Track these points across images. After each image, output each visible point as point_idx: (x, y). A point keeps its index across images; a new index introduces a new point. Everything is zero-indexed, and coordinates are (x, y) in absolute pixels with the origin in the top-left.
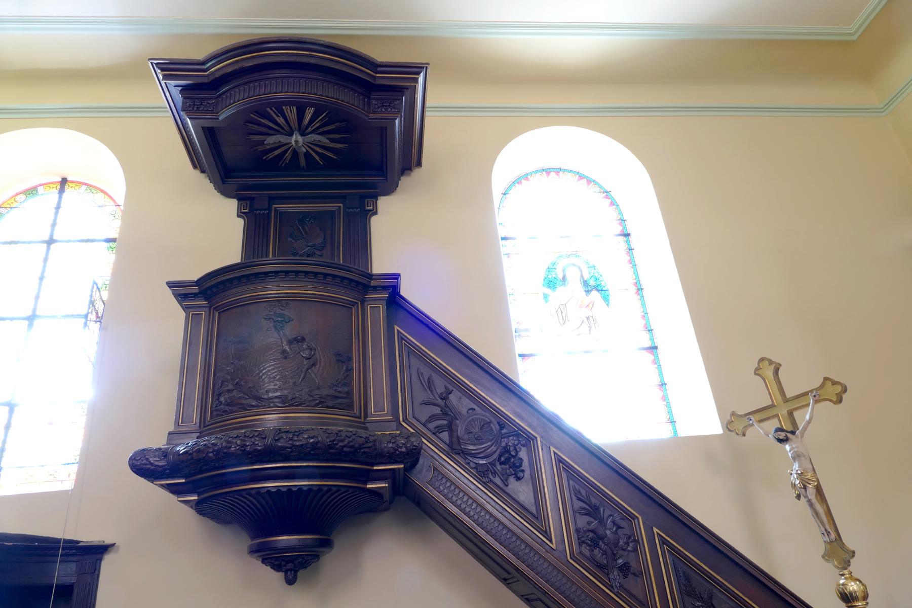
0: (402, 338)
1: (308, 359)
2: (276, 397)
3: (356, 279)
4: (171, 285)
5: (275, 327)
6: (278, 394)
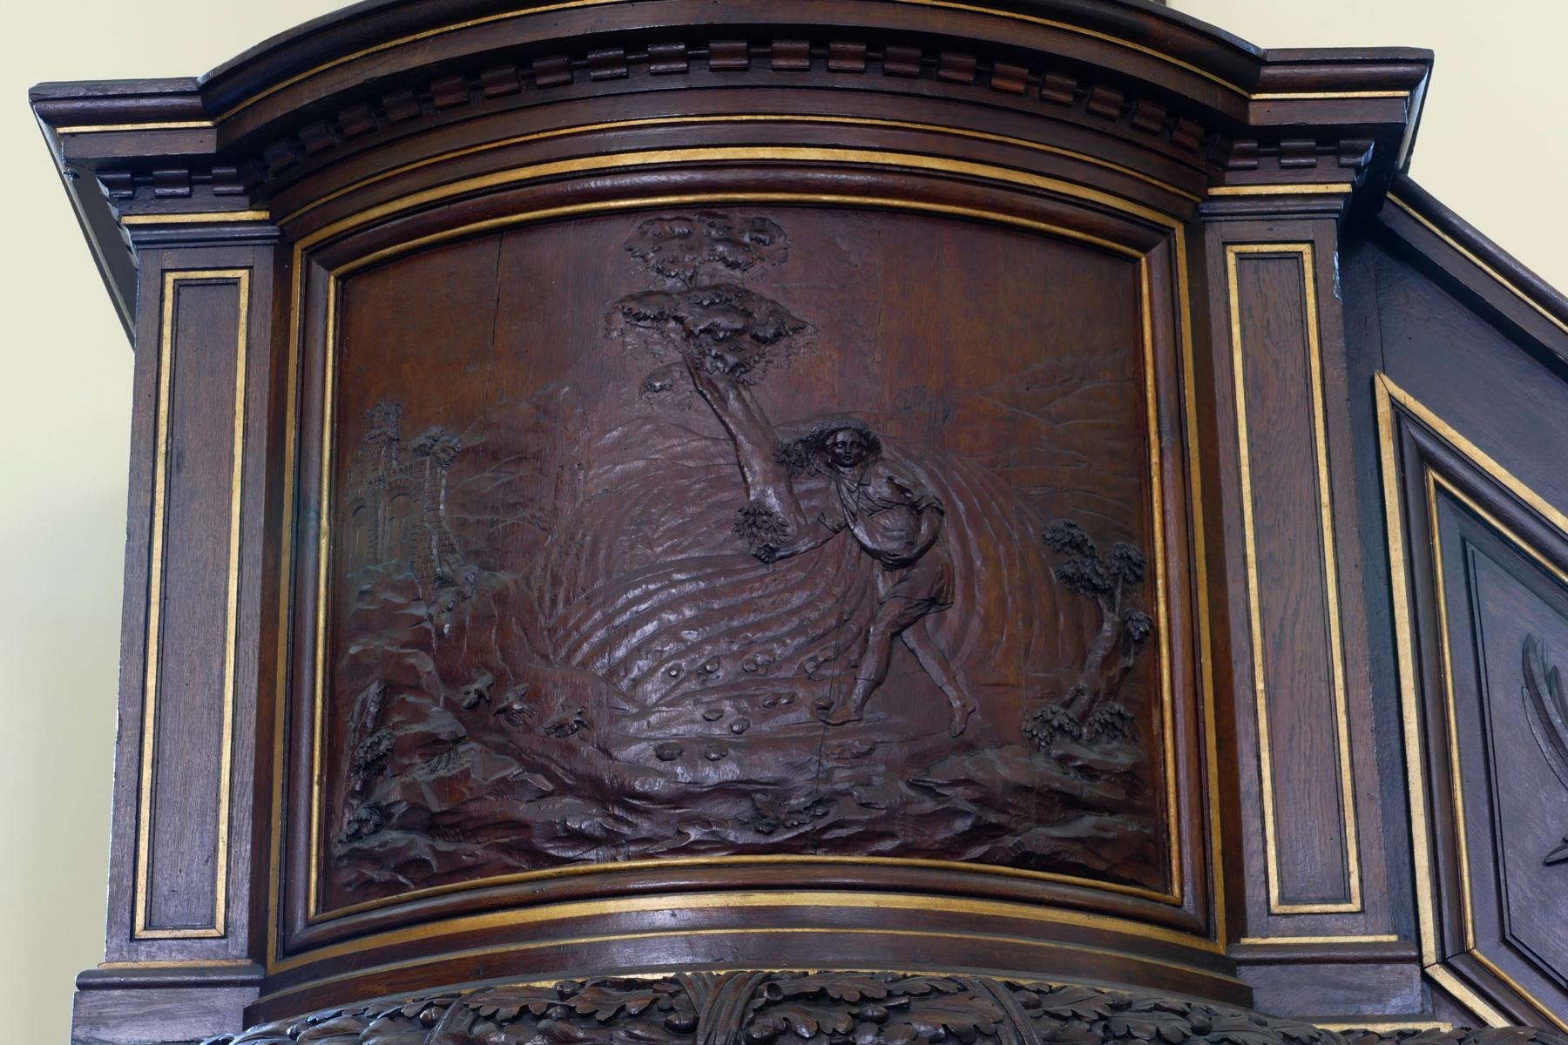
0: (1422, 456)
1: (895, 564)
2: (724, 790)
3: (1171, 82)
4: (58, 107)
5: (694, 369)
6: (729, 771)
